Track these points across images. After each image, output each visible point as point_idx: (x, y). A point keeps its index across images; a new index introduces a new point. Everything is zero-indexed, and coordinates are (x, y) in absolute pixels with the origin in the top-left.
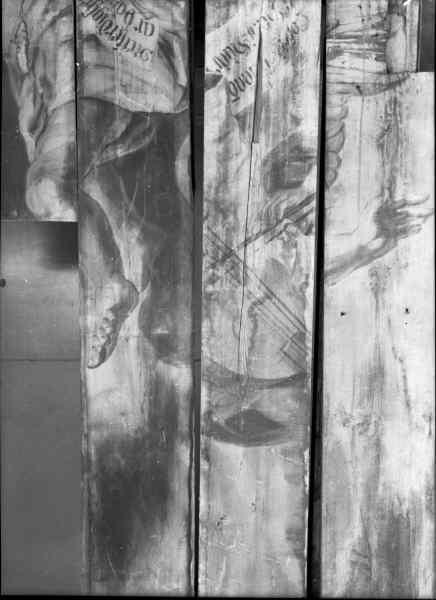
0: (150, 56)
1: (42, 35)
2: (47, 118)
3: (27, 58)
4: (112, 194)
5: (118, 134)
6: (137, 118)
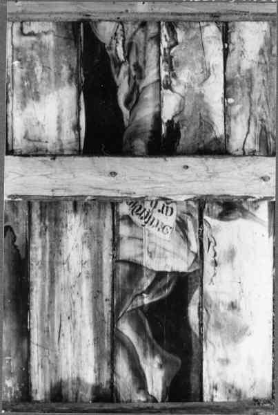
0: (170, 231)
1: (134, 34)
2: (139, 94)
3: (124, 50)
4: (140, 330)
5: (145, 288)
6: (160, 275)
